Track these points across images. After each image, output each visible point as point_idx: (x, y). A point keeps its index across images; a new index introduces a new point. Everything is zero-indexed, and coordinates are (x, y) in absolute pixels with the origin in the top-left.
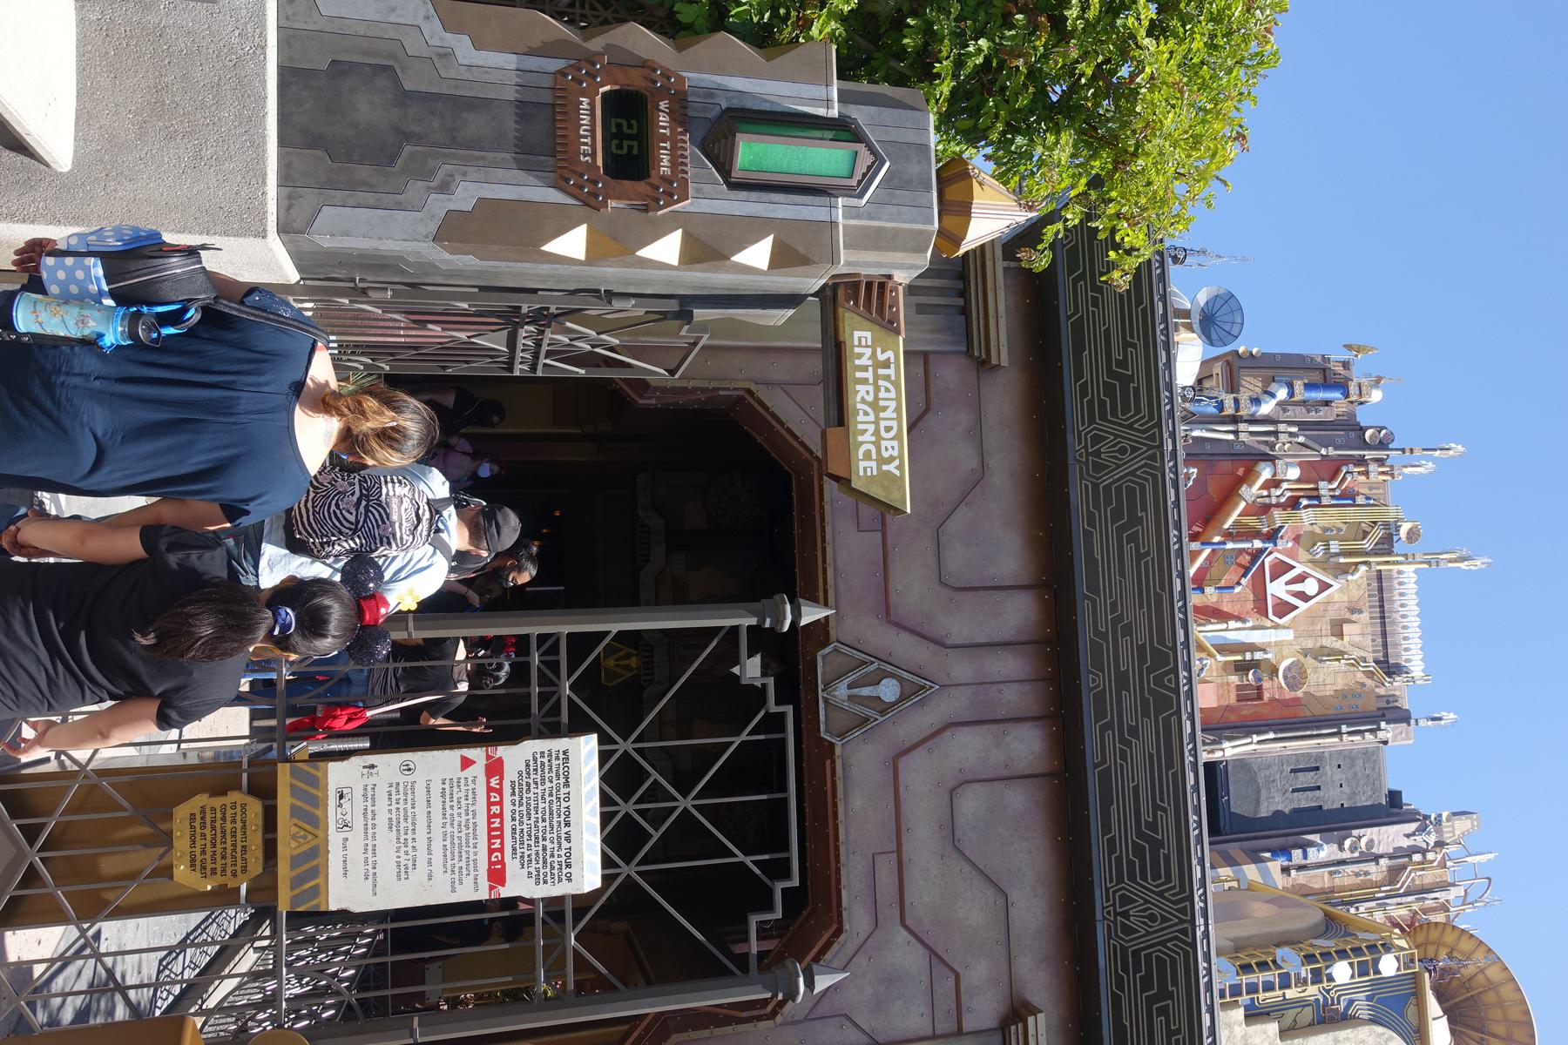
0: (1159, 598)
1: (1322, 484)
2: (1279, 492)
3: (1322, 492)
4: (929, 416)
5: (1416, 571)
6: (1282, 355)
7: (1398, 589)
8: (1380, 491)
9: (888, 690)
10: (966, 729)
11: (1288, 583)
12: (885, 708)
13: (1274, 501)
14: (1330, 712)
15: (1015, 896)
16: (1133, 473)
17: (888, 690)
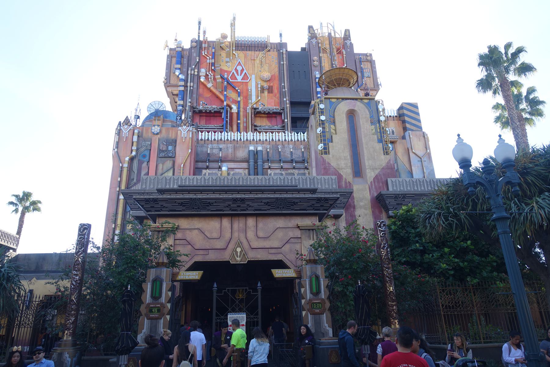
0: (223, 200)
1: (208, 61)
3: (211, 62)
4: (187, 239)
6: (166, 70)
8: (211, 44)
9: (239, 250)
10: (247, 235)
11: (238, 75)
12: (242, 251)
13: (212, 77)
14: (277, 66)
15: (278, 226)
16: (200, 203)
17: (239, 250)
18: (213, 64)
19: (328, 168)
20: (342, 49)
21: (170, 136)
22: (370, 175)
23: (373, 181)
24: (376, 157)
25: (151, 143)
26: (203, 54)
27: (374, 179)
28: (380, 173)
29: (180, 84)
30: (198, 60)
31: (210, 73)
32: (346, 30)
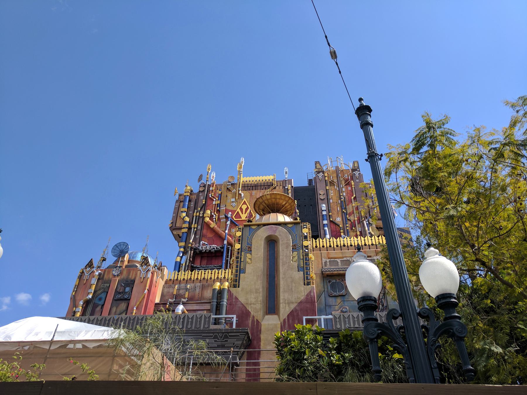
1: (214, 203)
2: (215, 215)
3: (216, 203)
5: (243, 177)
7: (248, 182)
8: (219, 186)
11: (242, 214)
13: (217, 217)
18: (219, 205)
19: (234, 303)
20: (351, 180)
21: (130, 277)
22: (285, 310)
23: (286, 318)
24: (293, 290)
25: (110, 285)
26: (210, 196)
27: (288, 316)
28: (297, 308)
29: (184, 226)
30: (204, 203)
31: (215, 213)
32: (354, 162)
